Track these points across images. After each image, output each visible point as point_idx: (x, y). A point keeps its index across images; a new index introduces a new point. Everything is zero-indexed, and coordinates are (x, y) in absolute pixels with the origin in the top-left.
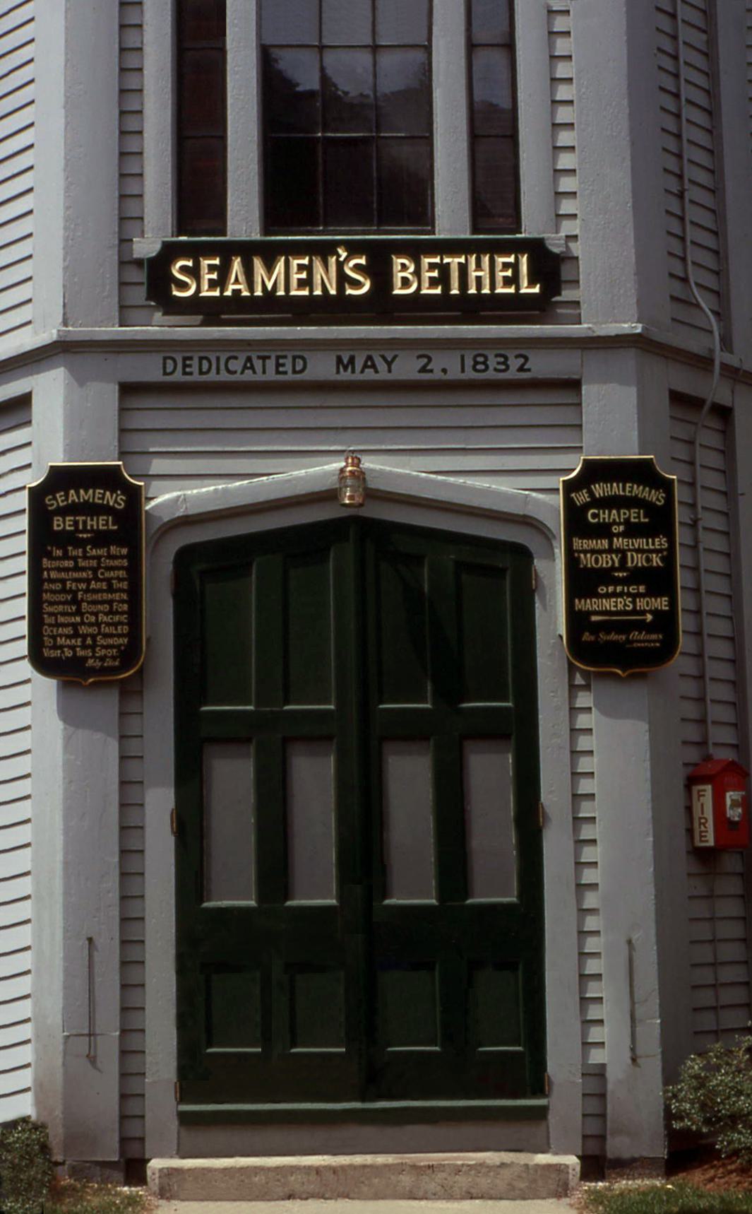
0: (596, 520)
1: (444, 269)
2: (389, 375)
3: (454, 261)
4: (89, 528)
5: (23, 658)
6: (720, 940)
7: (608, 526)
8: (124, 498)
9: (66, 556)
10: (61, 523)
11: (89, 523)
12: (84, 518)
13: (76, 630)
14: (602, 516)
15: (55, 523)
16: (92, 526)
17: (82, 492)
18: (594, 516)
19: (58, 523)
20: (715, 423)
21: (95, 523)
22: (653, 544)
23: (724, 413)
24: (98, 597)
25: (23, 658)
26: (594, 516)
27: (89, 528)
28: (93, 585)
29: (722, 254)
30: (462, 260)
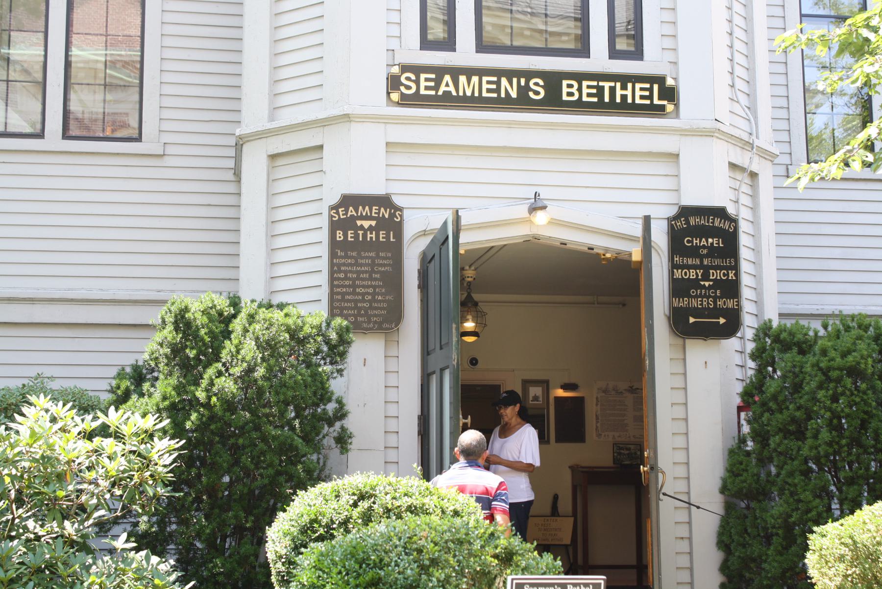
0: (690, 244)
1: (601, 90)
2: (137, 358)
3: (607, 85)
4: (618, 100)
5: (6, 128)
6: (8, 84)
7: (698, 248)
8: (395, 219)
9: (346, 257)
10: (574, 90)
11: (619, 92)
12: (612, 84)
13: (356, 305)
14: (695, 241)
15: (565, 90)
16: (624, 97)
17: (382, 210)
18: (688, 241)
19: (570, 90)
20: (747, 180)
21: (629, 92)
22: (726, 263)
23: (753, 175)
24: (366, 283)
25: (6, 128)
26: (688, 241)
27: (618, 100)
28: (355, 276)
29: (751, 82)
30: (612, 84)
